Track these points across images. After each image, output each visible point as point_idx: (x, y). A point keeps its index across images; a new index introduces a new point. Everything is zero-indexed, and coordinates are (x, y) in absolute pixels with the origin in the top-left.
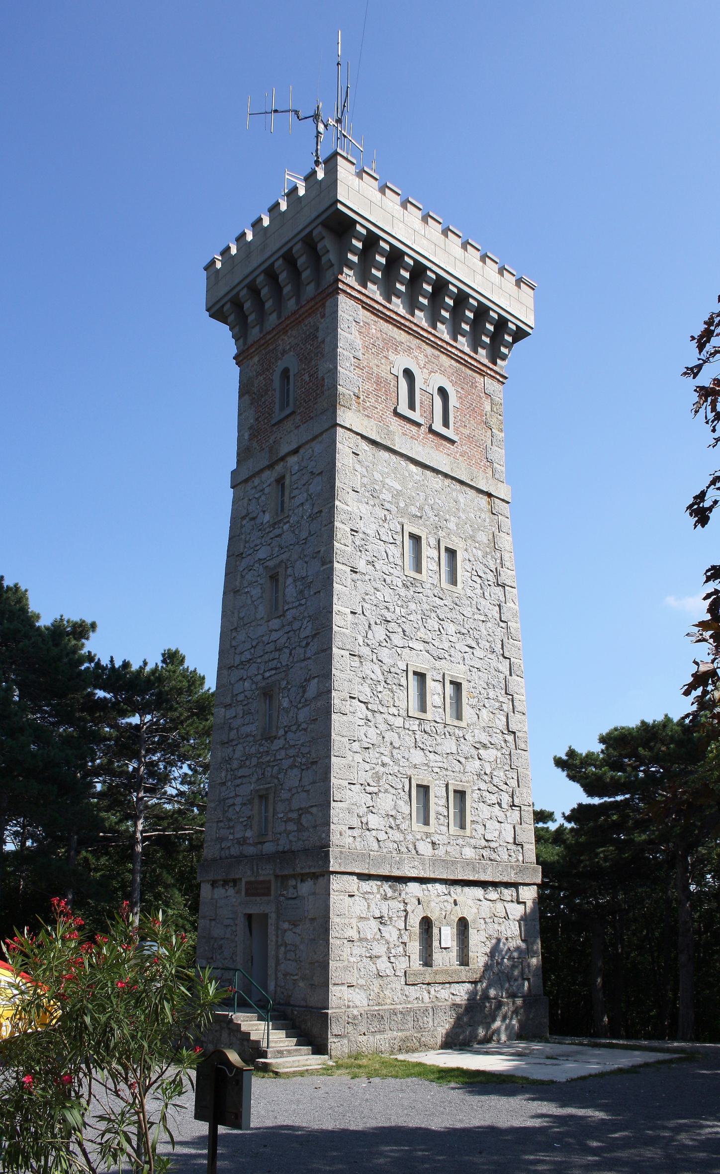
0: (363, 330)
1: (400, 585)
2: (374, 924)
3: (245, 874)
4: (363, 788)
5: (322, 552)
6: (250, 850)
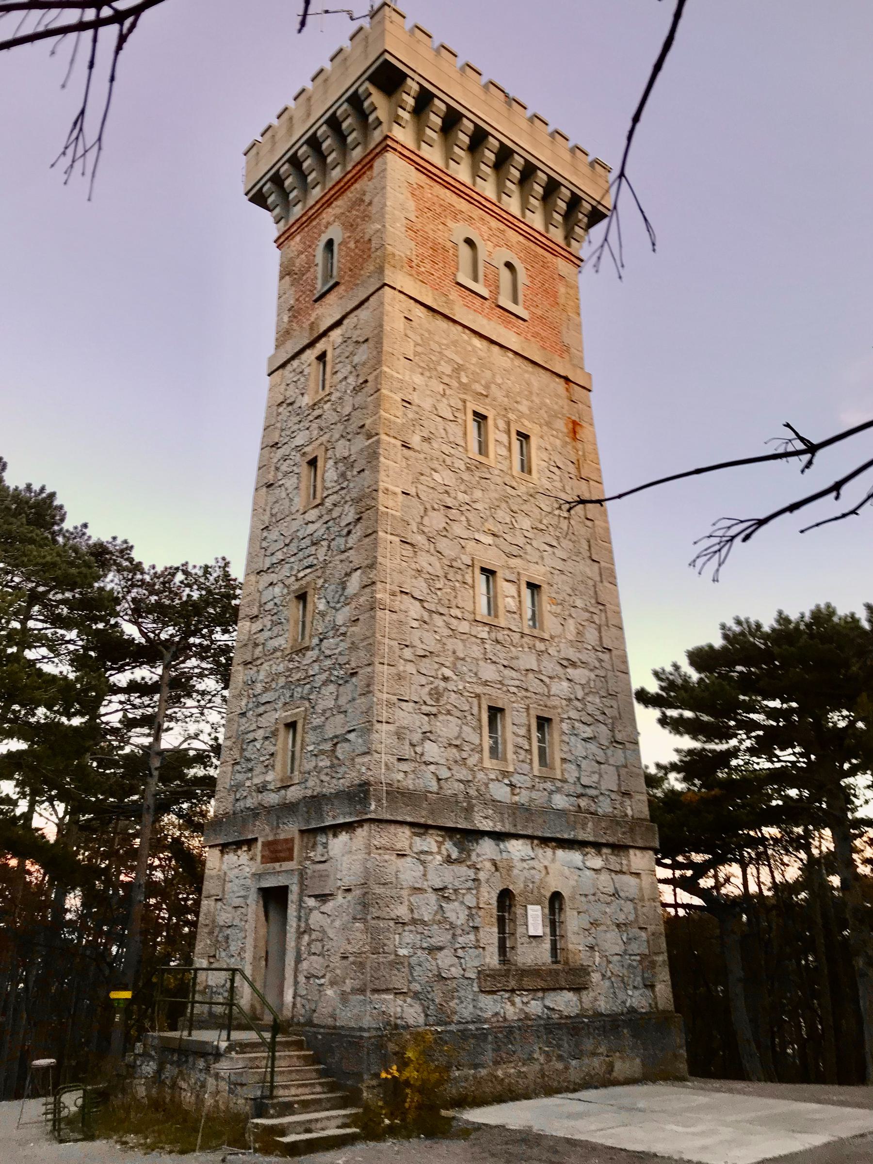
0: (417, 193)
1: (463, 468)
2: (432, 897)
3: (262, 832)
4: (417, 706)
5: (367, 426)
6: (272, 799)
